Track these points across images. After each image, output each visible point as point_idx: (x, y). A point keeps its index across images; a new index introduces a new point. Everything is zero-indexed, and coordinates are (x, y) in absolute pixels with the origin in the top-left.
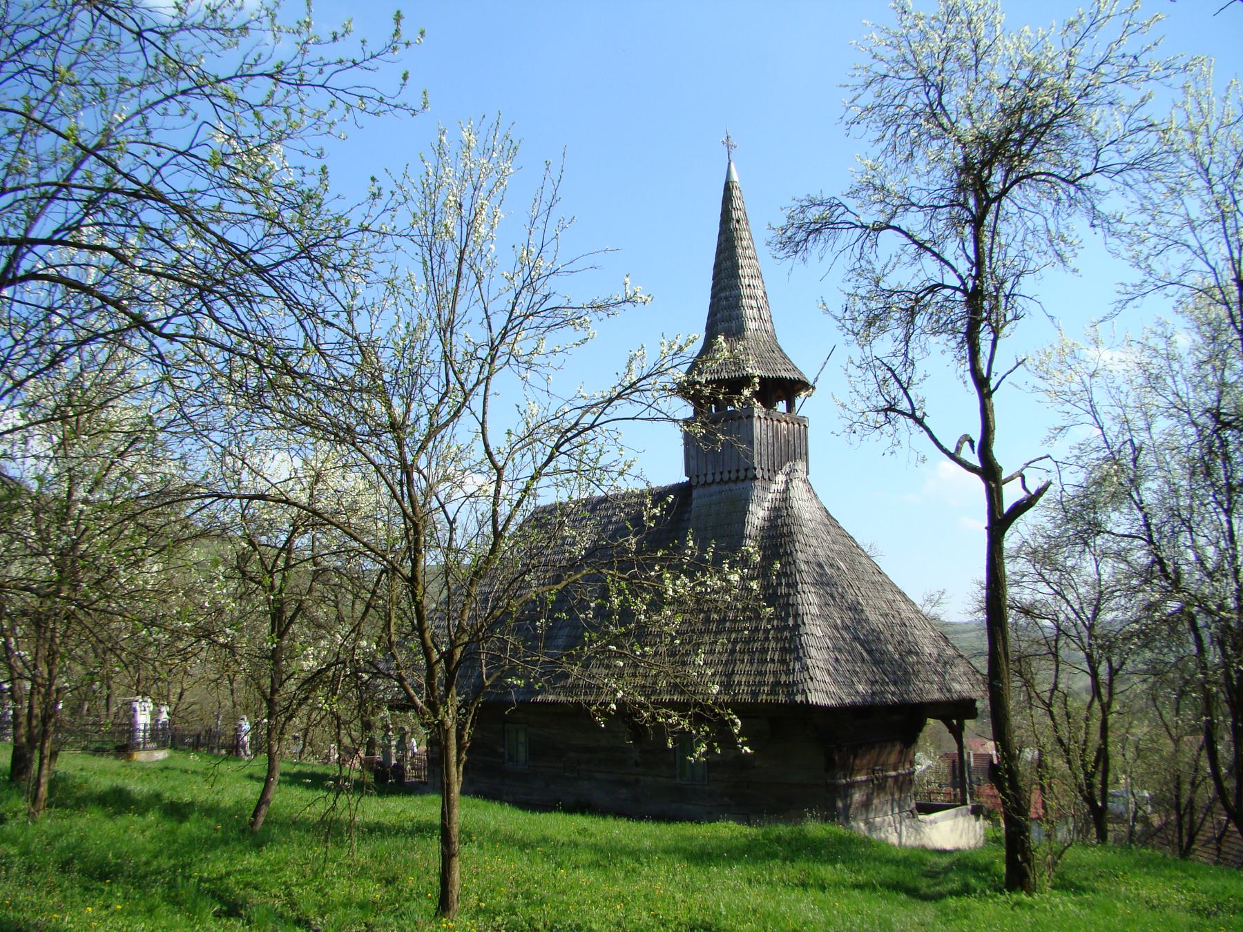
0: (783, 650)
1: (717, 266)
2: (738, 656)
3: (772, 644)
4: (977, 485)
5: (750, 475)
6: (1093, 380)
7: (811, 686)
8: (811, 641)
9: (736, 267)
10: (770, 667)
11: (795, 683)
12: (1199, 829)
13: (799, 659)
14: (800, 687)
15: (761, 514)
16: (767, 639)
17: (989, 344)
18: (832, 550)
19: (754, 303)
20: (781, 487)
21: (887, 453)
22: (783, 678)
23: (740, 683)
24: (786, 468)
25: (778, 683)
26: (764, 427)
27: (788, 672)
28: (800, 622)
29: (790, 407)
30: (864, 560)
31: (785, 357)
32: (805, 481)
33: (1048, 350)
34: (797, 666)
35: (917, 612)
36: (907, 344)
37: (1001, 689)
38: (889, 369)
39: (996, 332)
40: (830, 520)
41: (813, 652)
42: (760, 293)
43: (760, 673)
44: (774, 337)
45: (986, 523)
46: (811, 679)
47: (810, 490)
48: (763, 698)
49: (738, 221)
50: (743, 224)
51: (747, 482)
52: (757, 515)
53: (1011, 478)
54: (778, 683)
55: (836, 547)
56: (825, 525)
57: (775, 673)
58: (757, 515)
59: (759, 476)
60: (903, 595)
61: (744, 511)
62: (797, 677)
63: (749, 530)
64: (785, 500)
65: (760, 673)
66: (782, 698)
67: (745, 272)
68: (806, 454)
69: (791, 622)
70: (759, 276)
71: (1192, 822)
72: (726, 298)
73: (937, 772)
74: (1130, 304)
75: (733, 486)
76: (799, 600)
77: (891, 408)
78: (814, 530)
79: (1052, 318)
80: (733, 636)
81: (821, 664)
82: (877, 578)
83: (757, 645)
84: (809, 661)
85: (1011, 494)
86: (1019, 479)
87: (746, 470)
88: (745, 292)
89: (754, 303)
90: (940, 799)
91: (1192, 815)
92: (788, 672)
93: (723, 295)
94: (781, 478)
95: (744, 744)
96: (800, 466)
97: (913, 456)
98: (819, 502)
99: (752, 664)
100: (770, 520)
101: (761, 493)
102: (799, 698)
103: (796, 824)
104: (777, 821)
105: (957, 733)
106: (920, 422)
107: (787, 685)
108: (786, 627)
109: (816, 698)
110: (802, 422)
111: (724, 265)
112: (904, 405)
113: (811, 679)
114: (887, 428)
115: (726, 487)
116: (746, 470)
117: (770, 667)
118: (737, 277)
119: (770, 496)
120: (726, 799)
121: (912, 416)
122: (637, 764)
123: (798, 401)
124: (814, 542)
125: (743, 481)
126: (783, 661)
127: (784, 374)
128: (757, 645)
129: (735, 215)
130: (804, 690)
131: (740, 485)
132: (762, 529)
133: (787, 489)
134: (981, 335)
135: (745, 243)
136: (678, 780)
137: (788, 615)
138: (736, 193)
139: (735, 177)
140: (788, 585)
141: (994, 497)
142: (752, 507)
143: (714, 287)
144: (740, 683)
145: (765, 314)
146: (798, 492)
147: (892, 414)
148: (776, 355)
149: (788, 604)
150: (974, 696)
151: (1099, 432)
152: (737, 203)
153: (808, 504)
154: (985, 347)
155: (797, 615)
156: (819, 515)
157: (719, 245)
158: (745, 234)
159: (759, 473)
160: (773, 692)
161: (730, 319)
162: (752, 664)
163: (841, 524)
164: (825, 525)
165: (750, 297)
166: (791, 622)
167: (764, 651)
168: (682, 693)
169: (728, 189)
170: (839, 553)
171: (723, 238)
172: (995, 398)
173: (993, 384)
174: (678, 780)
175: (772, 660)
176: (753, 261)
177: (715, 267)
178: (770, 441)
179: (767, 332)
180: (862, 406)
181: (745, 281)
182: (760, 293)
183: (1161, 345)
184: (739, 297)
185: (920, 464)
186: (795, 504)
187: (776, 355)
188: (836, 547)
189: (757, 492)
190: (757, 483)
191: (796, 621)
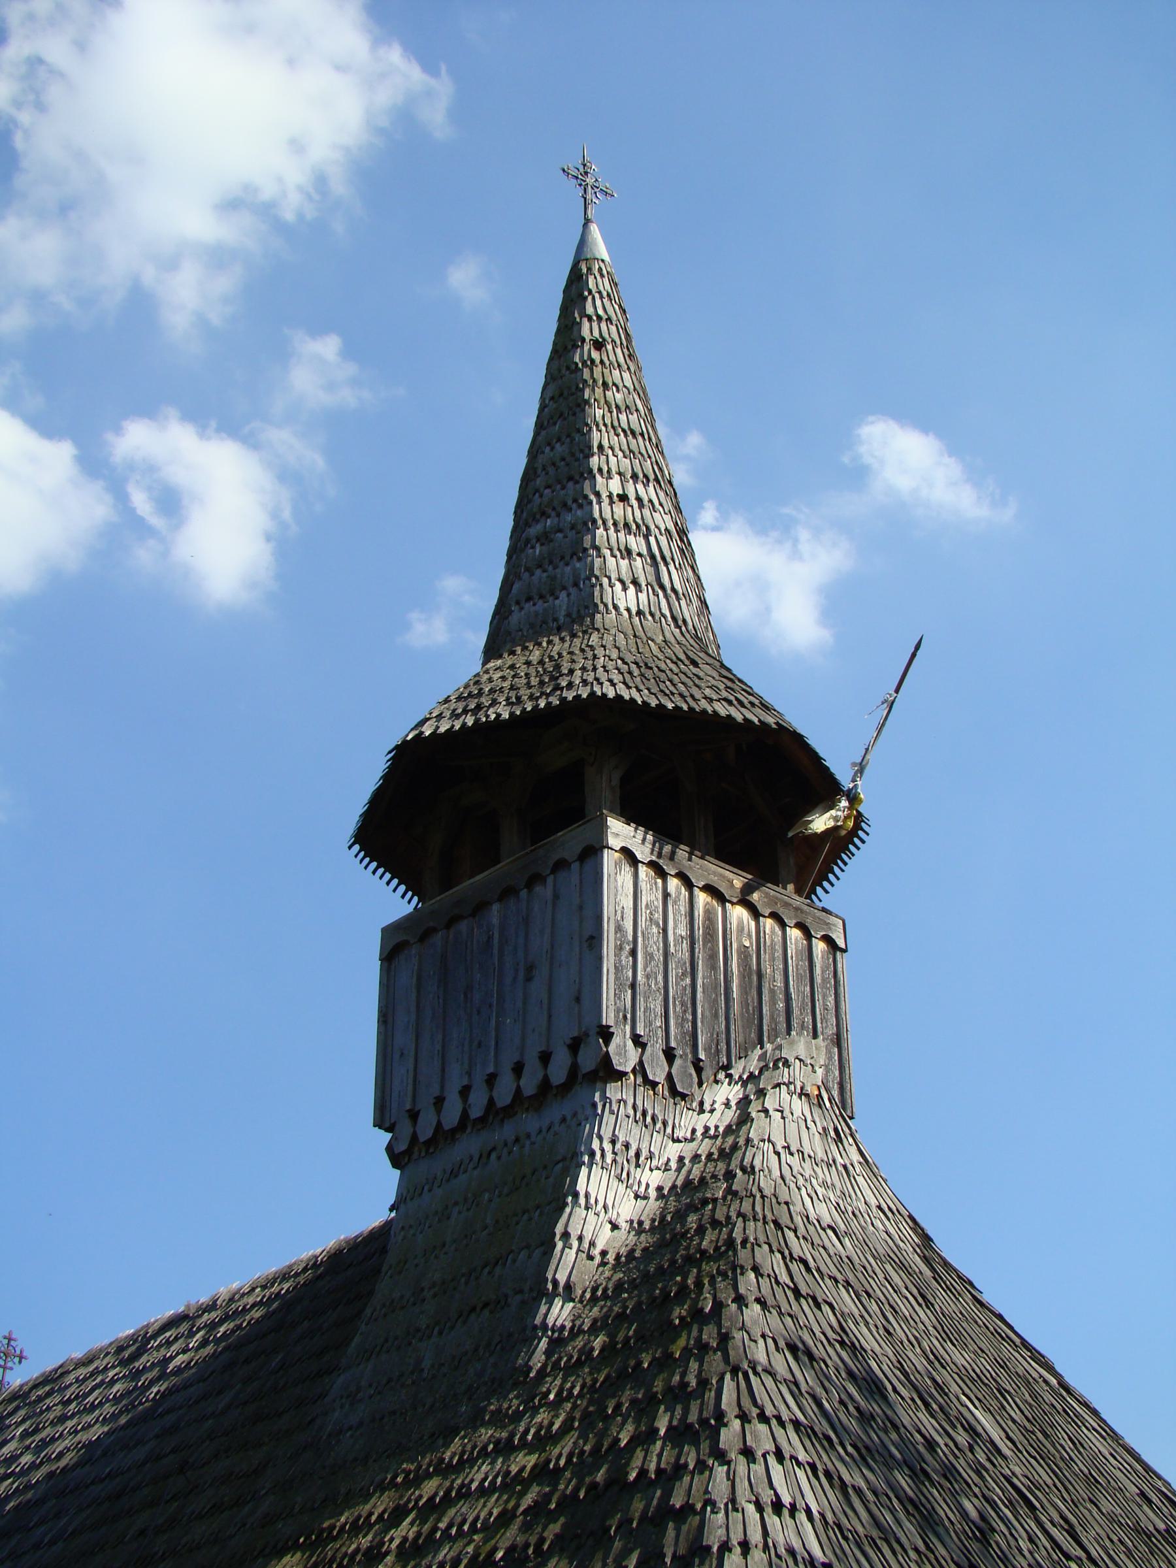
15: (627, 1209)
19: (636, 543)
20: (721, 1118)
49: (599, 345)
87: (575, 1046)
88: (602, 510)
89: (636, 543)
93: (535, 530)
100: (660, 1225)
101: (630, 1133)
119: (673, 1151)
125: (567, 1087)
132: (626, 1260)
145: (674, 577)
159: (623, 1054)
178: (681, 952)
190: (613, 1091)
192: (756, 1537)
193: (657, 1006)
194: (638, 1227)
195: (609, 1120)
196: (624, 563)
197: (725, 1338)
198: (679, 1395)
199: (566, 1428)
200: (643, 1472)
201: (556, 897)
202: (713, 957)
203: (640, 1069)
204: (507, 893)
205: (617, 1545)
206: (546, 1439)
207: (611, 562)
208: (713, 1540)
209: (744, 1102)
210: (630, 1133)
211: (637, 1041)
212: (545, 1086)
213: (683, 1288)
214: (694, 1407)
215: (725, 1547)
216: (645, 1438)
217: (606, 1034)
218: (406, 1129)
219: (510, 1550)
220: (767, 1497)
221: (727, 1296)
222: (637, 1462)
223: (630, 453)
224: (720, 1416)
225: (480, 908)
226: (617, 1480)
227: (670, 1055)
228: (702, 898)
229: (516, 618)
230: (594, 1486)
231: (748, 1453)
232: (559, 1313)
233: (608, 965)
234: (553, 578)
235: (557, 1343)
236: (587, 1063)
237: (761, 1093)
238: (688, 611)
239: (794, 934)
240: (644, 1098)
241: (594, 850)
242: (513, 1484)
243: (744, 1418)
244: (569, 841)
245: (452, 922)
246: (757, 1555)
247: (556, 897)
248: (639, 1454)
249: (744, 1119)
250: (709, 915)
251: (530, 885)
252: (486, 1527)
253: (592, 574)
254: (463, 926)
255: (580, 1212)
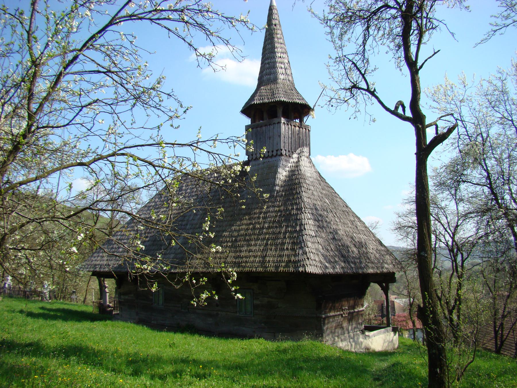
0: (293, 243)
1: (264, 49)
2: (269, 247)
3: (288, 240)
4: (410, 129)
5: (279, 153)
6: (462, 104)
7: (308, 262)
8: (308, 238)
9: (274, 47)
10: (286, 252)
11: (299, 261)
12: (506, 338)
13: (301, 248)
14: (302, 263)
15: (285, 173)
16: (285, 237)
17: (416, 46)
18: (322, 193)
19: (283, 66)
20: (295, 160)
21: (352, 118)
22: (293, 259)
23: (269, 261)
24: (298, 151)
25: (290, 261)
26: (287, 128)
27: (295, 255)
28: (303, 228)
29: (301, 121)
30: (339, 200)
31: (298, 93)
32: (308, 157)
33: (440, 87)
34: (301, 252)
35: (366, 227)
36: (364, 47)
37: (427, 257)
38: (353, 63)
39: (421, 35)
40: (321, 178)
41: (309, 244)
42: (286, 61)
43: (280, 256)
44: (293, 84)
45: (415, 151)
46: (308, 258)
47: (311, 162)
48: (281, 269)
49: (275, 25)
50: (278, 27)
51: (278, 157)
52: (282, 174)
53: (430, 125)
54: (290, 261)
55: (324, 192)
56: (318, 180)
57: (288, 256)
58: (282, 174)
59: (284, 154)
60: (359, 218)
61: (276, 172)
62: (300, 257)
63: (278, 182)
64: (297, 167)
65: (280, 256)
66: (291, 269)
67: (278, 50)
68: (309, 145)
69: (298, 228)
70: (286, 53)
71: (502, 335)
72: (268, 63)
73: (372, 310)
74: (497, 33)
75: (270, 160)
76: (303, 217)
77: (355, 86)
78: (312, 182)
79: (453, 34)
80: (267, 236)
81: (314, 251)
82: (344, 209)
83: (280, 241)
84: (307, 249)
85: (430, 134)
86: (434, 127)
87: (277, 151)
88: (278, 60)
89: (283, 66)
90: (375, 323)
91: (502, 331)
92: (295, 255)
93: (267, 62)
94: (295, 156)
95: (236, 292)
96: (306, 149)
97: (368, 118)
98: (315, 168)
99: (276, 251)
100: (289, 176)
101: (284, 163)
102: (301, 269)
103: (297, 341)
104: (287, 339)
105: (386, 290)
106: (373, 93)
107: (295, 262)
108: (296, 231)
109: (310, 269)
110: (307, 128)
111: (268, 47)
112: (363, 85)
113: (308, 258)
114: (352, 101)
115: (267, 160)
116: (277, 151)
117: (286, 252)
118: (275, 53)
119: (289, 165)
120: (263, 324)
121: (368, 90)
122: (217, 305)
123: (305, 119)
124: (312, 188)
125: (275, 156)
126: (293, 249)
127: (298, 101)
128: (280, 241)
129: (274, 22)
130: (303, 265)
131: (274, 159)
132: (285, 181)
133: (298, 161)
134: (411, 37)
135: (279, 36)
136: (238, 314)
137: (296, 225)
138: (274, 11)
139: (274, 3)
140: (297, 209)
141: (420, 134)
142: (280, 170)
143: (262, 58)
144: (269, 261)
145: (288, 72)
146: (304, 163)
147: (354, 91)
148: (294, 92)
149: (297, 219)
150: (395, 271)
151: (464, 130)
152: (275, 16)
153: (309, 169)
154: (413, 39)
155: (301, 225)
156: (315, 175)
157: (266, 37)
158: (279, 32)
159: (284, 152)
160: (287, 266)
161: (270, 74)
162: (276, 251)
163: (327, 181)
164: (318, 180)
165: (281, 63)
166: (298, 228)
167: (283, 244)
168: (239, 267)
169: (271, 9)
170: (325, 195)
171: (268, 33)
172: (421, 73)
173: (419, 64)
174: (238, 314)
175: (287, 249)
176: (282, 45)
177: (263, 48)
178: (290, 136)
179: (289, 81)
180: (336, 87)
181: (279, 55)
182: (286, 61)
183: (499, 84)
184: (275, 62)
185: (372, 123)
186: (302, 168)
187: (294, 92)
188: (324, 192)
189: (283, 162)
190: (282, 157)
191: (300, 228)
192: (307, 223)
193: (288, 145)
194: (286, 176)
195: (282, 161)
196: (281, 70)
197: (301, 197)
198: (296, 204)
199: (282, 205)
200: (293, 214)
201: (274, 128)
202: (294, 136)
203: (286, 154)
204: (266, 125)
205: (292, 222)
206: (279, 206)
207: (279, 70)
208: (303, 223)
209: (298, 158)
210: (284, 163)
211: (285, 150)
212: (273, 155)
213: (294, 188)
214: (298, 206)
215: (305, 224)
216: (293, 209)
217: (282, 150)
218: (251, 156)
219: (278, 220)
220: (308, 218)
221: (300, 191)
222: (292, 212)
223: (281, 48)
224: (302, 208)
225: (261, 127)
226: (290, 214)
227: (289, 151)
228: (293, 127)
229: (265, 78)
230: (287, 214)
231: (305, 213)
232: (277, 188)
233: (282, 140)
234: (270, 72)
235: (277, 192)
236: (279, 153)
237: (301, 157)
238: (290, 78)
239: (304, 130)
240: (286, 158)
241: (279, 123)
242: (276, 212)
243: (304, 208)
244: (276, 120)
245: (257, 128)
246: (308, 225)
247: (274, 128)
248: (292, 211)
249: (299, 161)
250: (294, 129)
251: (270, 125)
252: (274, 217)
253: (276, 72)
254: (259, 129)
255: (279, 174)
